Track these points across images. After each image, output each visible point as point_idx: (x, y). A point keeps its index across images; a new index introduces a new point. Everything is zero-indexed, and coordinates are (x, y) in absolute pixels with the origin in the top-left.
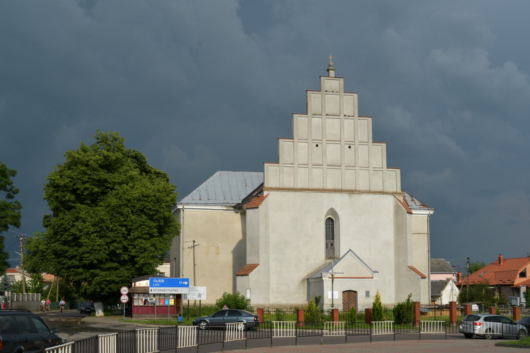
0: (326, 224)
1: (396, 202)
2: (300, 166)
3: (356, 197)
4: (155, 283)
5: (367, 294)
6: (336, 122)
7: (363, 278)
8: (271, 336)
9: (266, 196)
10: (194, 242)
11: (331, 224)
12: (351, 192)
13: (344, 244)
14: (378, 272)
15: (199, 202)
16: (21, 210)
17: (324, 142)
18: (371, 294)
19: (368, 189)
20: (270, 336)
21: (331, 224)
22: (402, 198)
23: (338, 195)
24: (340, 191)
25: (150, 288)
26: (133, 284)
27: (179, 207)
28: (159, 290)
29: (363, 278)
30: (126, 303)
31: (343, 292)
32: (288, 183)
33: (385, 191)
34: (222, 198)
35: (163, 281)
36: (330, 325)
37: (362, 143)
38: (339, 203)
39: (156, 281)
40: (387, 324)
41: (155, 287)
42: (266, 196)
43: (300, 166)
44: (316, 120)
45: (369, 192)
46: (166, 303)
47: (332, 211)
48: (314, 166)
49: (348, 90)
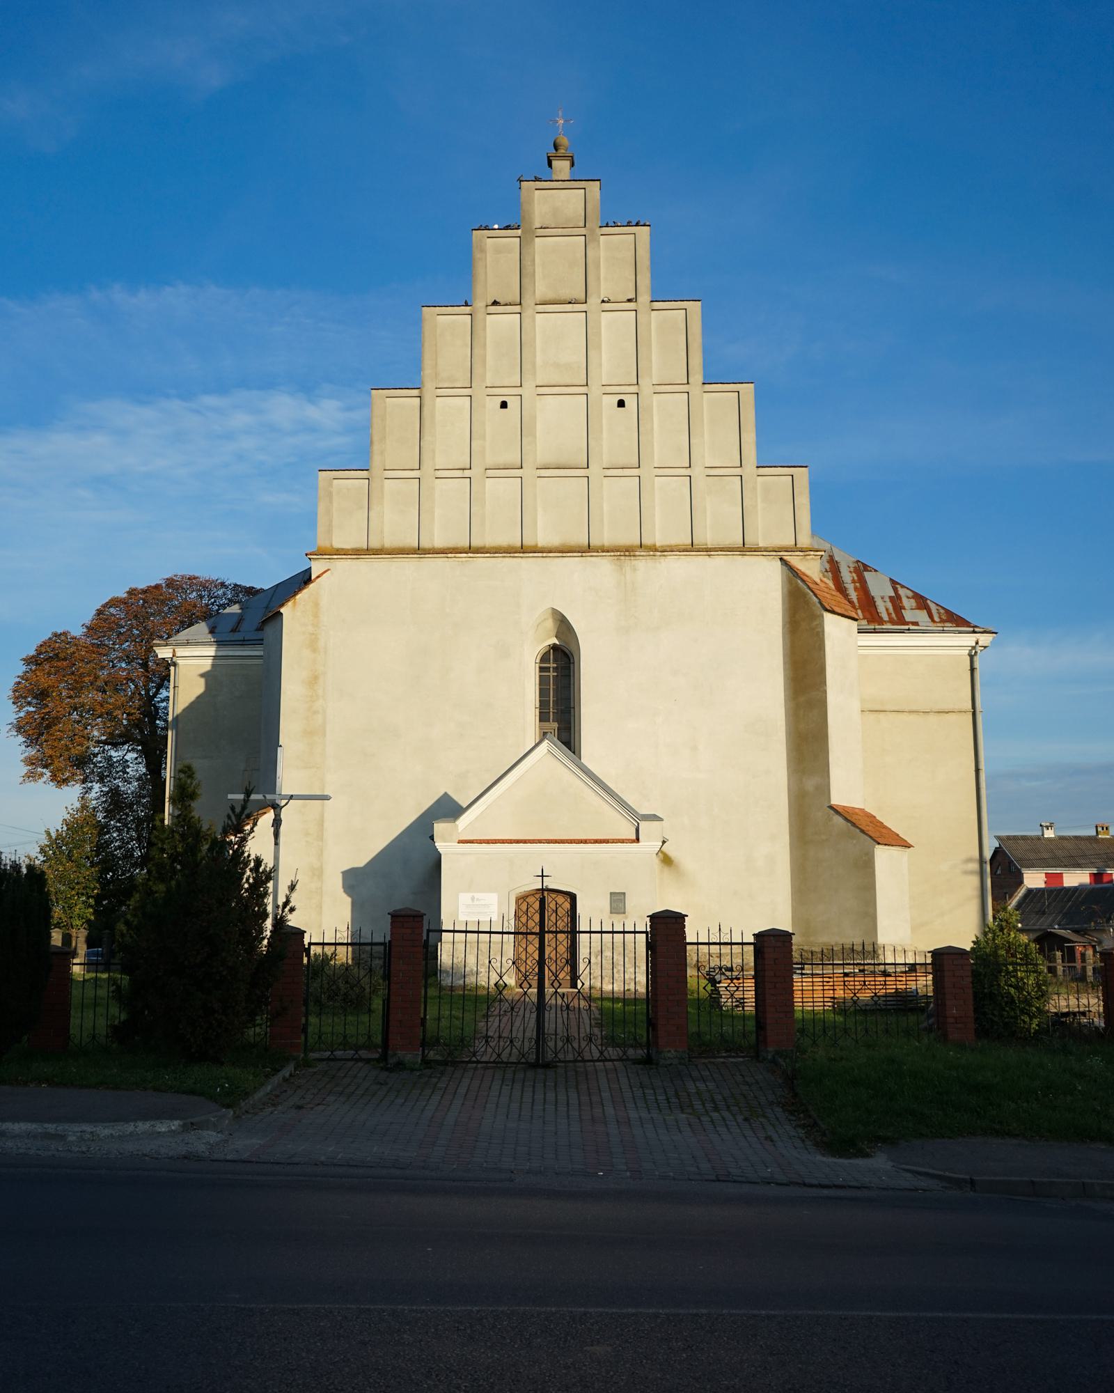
0: (542, 669)
1: (790, 582)
2: (439, 474)
3: (642, 566)
5: (618, 902)
6: (572, 321)
7: (596, 841)
10: (664, 842)
11: (560, 668)
12: (627, 551)
14: (661, 820)
16: (13, 718)
17: (528, 391)
18: (630, 903)
21: (560, 668)
23: (573, 563)
24: (587, 550)
29: (596, 841)
31: (572, 898)
32: (395, 527)
37: (662, 387)
38: (583, 592)
43: (439, 474)
44: (501, 324)
45: (692, 548)
46: (912, 986)
47: (563, 626)
49: (613, 218)
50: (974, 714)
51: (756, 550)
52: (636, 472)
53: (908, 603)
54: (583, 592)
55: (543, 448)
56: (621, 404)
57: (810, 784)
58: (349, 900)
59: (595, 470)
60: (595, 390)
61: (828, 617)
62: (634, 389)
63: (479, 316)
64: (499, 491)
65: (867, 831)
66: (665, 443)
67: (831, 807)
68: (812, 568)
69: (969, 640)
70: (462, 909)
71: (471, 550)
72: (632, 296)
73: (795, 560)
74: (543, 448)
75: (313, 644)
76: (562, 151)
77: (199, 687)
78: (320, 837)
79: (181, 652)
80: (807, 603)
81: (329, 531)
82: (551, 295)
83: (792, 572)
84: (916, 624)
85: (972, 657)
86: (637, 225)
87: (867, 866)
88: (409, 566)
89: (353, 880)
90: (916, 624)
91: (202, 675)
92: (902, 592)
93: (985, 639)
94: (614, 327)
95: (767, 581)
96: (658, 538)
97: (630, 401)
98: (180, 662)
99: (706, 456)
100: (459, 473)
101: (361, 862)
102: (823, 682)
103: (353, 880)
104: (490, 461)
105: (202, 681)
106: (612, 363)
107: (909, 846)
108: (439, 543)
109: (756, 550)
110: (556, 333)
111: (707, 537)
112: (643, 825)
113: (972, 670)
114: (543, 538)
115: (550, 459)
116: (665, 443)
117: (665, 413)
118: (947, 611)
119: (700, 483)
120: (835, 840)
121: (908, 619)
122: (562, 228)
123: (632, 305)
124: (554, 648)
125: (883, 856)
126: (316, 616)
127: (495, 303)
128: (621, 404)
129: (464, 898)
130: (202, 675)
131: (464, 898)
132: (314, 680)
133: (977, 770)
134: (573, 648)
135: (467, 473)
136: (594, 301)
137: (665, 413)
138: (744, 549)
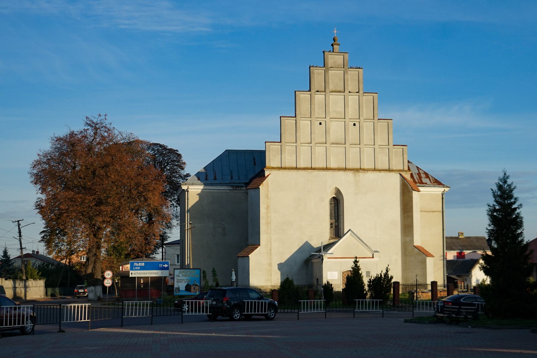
1: (402, 181)
3: (361, 174)
4: (135, 266)
8: (60, 321)
9: (268, 176)
11: (337, 203)
13: (349, 222)
15: (214, 182)
19: (402, 168)
20: (58, 321)
21: (337, 203)
22: (409, 175)
23: (341, 173)
24: (345, 169)
25: (131, 272)
26: (121, 267)
27: (184, 187)
28: (140, 274)
30: (109, 287)
32: (289, 161)
33: (283, 166)
34: (229, 177)
35: (143, 264)
36: (140, 306)
38: (344, 182)
39: (137, 265)
40: (136, 305)
41: (136, 270)
42: (268, 176)
44: (319, 98)
45: (375, 170)
48: (332, 145)
50: (443, 212)
51: (393, 171)
52: (359, 146)
53: (423, 176)
54: (344, 182)
55: (332, 138)
56: (354, 125)
57: (408, 239)
58: (280, 272)
59: (347, 145)
60: (347, 120)
61: (414, 192)
62: (358, 120)
63: (313, 95)
64: (320, 150)
65: (423, 253)
66: (367, 137)
67: (415, 247)
68: (407, 176)
69: (441, 189)
70: (328, 276)
71: (312, 169)
72: (358, 91)
73: (403, 174)
74: (332, 138)
75: (267, 197)
76: (336, 42)
77: (197, 199)
78: (271, 254)
79: (190, 187)
80: (408, 187)
81: (270, 162)
82: (334, 89)
83: (403, 178)
84: (426, 184)
85: (442, 195)
86: (359, 68)
87: (424, 263)
88: (294, 173)
89: (281, 266)
90: (426, 184)
91: (198, 194)
92: (421, 171)
93: (447, 189)
94: (353, 99)
95: (395, 180)
96: (365, 166)
97: (357, 124)
98: (189, 190)
99: (379, 142)
100: (308, 145)
101: (283, 261)
102: (412, 211)
103: (281, 266)
104: (317, 141)
105: (198, 196)
106: (352, 111)
107: (433, 256)
108: (302, 166)
109: (393, 171)
110: (335, 100)
111: (379, 166)
112: (375, 254)
113: (443, 198)
114: (333, 165)
115: (334, 141)
116: (367, 137)
117: (367, 126)
118: (435, 179)
119: (377, 150)
120: (414, 255)
121: (424, 182)
122: (337, 67)
123: (358, 94)
124: (334, 197)
125: (429, 259)
126: (268, 188)
127: (317, 91)
128: (354, 125)
129: (329, 273)
130: (198, 194)
131: (329, 273)
132: (268, 208)
133: (443, 230)
134: (340, 198)
135: (310, 145)
136: (347, 92)
137: (367, 126)
138: (389, 170)
